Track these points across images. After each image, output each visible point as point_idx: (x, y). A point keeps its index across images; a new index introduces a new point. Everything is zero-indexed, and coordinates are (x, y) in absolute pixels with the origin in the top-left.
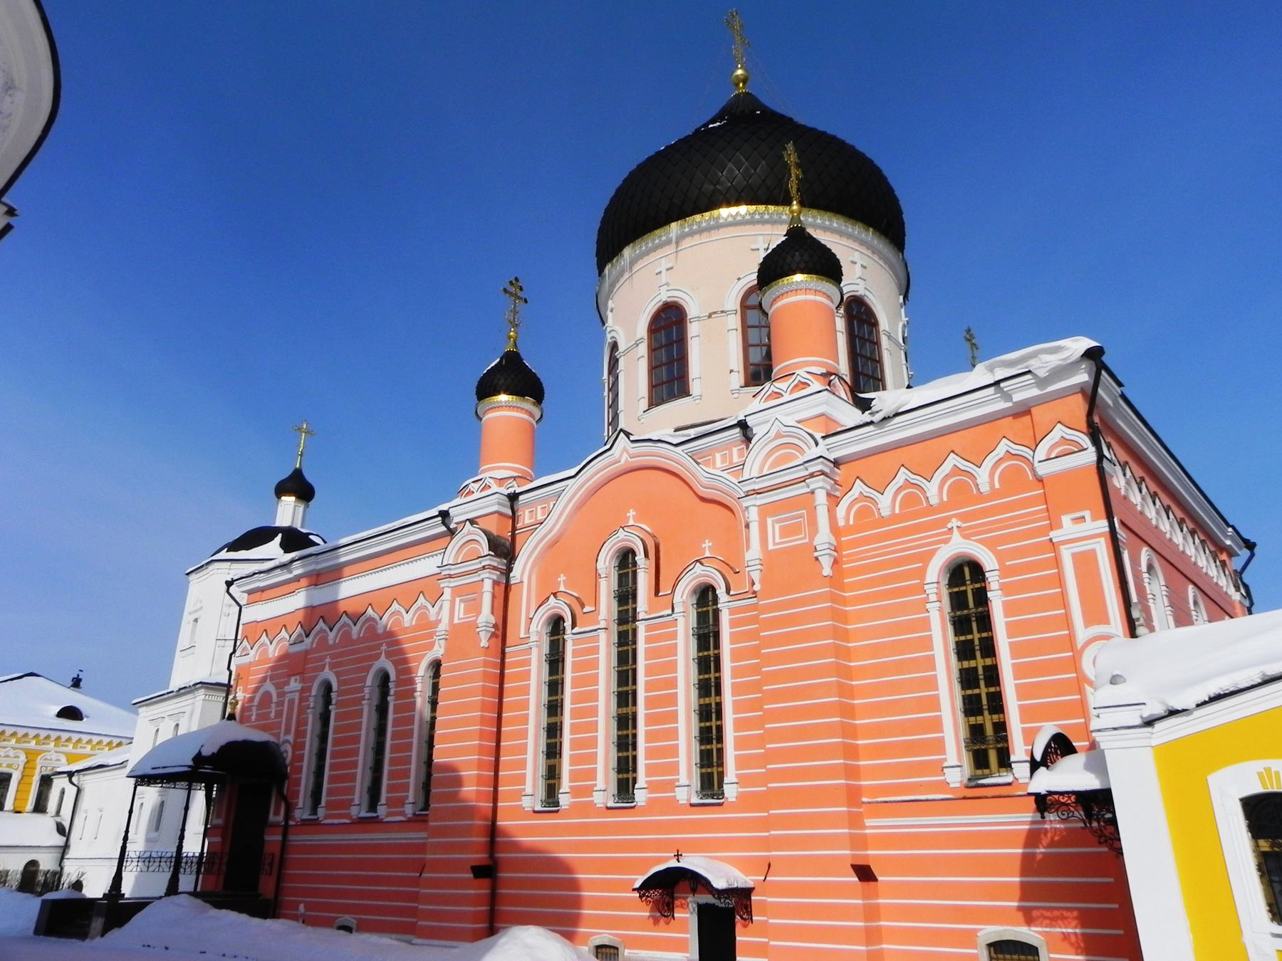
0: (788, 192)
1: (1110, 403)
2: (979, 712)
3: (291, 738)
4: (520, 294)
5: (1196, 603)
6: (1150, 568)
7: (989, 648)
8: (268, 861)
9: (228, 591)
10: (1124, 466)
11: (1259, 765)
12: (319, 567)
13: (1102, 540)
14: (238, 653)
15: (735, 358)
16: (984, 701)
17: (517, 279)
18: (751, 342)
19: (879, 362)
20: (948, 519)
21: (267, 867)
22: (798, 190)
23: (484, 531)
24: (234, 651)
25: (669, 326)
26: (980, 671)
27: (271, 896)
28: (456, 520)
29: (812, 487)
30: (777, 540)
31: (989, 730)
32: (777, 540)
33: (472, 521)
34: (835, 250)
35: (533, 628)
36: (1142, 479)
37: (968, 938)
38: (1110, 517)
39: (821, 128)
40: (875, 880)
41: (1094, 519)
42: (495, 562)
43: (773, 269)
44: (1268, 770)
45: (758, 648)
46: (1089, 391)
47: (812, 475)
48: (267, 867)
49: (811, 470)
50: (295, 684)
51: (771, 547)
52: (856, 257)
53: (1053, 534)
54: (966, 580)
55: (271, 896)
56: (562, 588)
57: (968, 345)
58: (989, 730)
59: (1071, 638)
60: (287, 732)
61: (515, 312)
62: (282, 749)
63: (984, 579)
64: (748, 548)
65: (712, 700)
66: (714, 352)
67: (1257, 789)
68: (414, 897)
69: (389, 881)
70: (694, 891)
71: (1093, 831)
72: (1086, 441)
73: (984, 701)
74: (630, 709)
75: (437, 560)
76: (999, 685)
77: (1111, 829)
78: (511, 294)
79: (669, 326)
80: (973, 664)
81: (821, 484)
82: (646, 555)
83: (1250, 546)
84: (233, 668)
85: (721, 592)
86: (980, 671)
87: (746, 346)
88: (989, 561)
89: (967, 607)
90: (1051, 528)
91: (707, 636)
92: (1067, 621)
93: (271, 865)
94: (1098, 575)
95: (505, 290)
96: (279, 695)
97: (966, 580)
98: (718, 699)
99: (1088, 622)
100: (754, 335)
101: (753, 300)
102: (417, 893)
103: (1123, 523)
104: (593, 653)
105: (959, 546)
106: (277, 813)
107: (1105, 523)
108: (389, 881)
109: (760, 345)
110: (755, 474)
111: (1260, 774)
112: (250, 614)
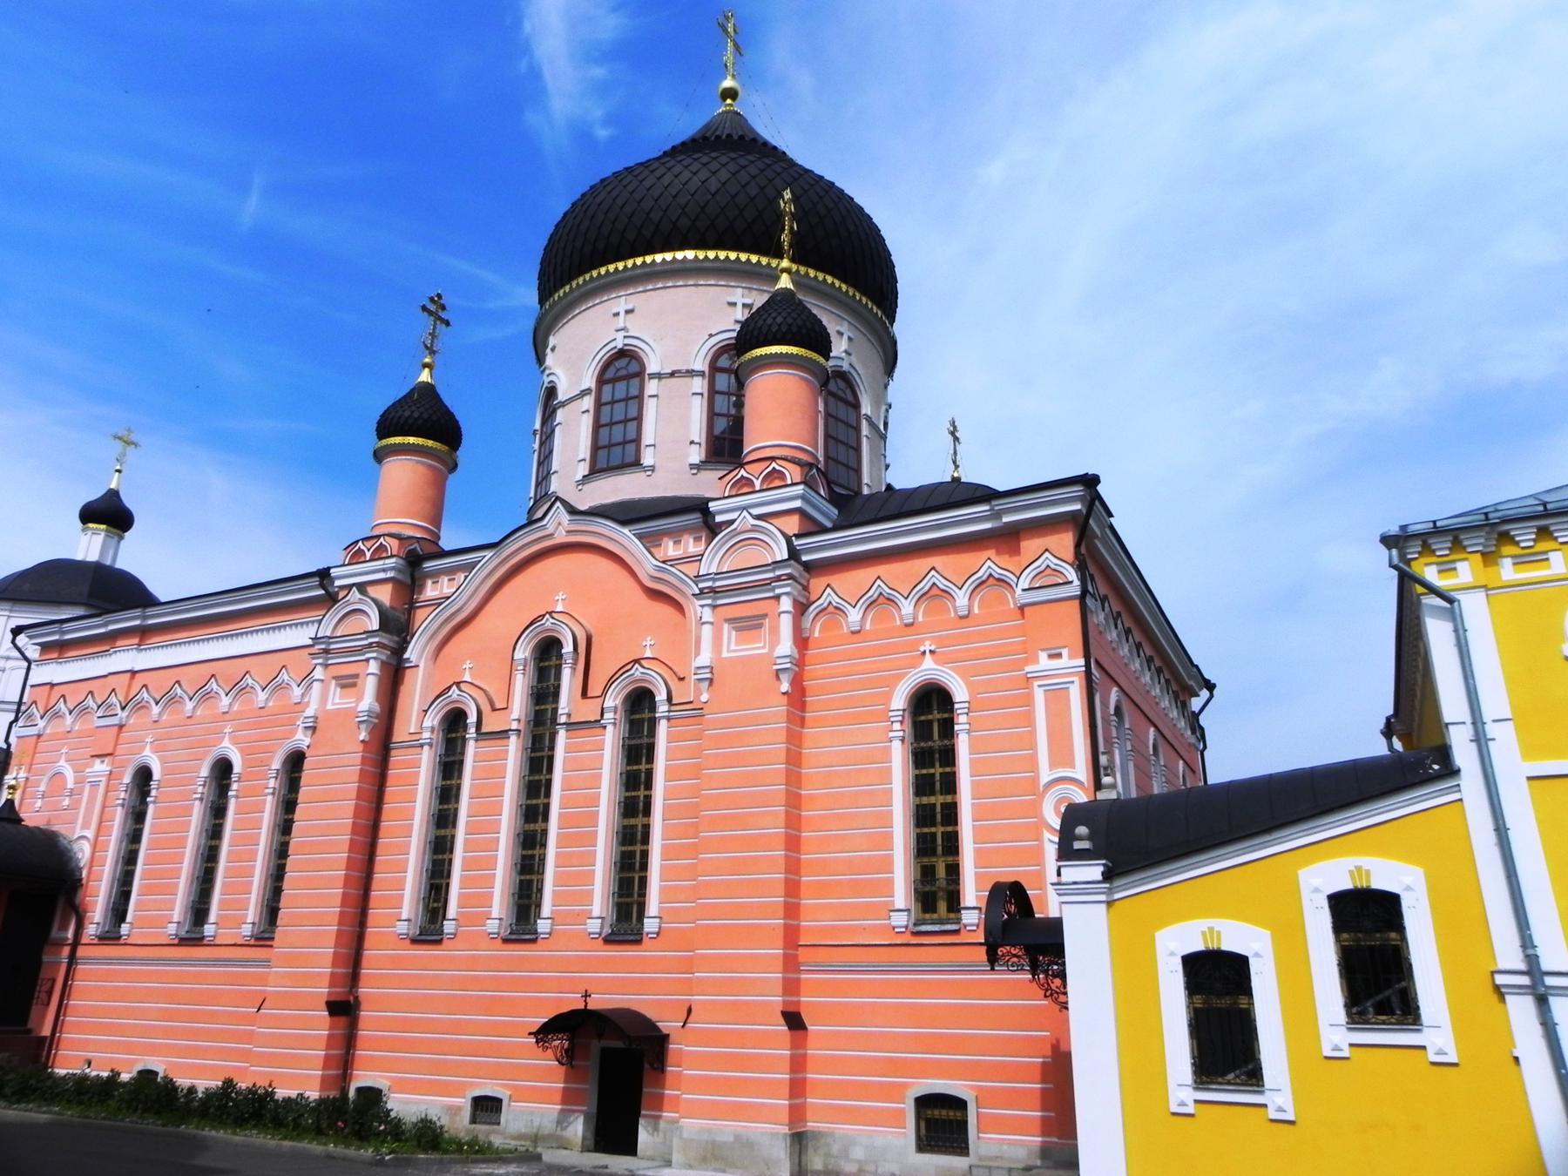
0: (780, 244)
1: (1098, 532)
2: (933, 853)
3: (90, 834)
4: (443, 315)
5: (1155, 747)
6: (1118, 710)
7: (950, 785)
8: (46, 988)
9: (13, 642)
10: (1104, 599)
11: (1203, 924)
12: (125, 658)
13: (1076, 679)
14: (20, 723)
15: (696, 427)
16: (939, 841)
17: (439, 296)
18: (717, 410)
19: (857, 450)
20: (921, 642)
21: (44, 996)
22: (791, 246)
23: (374, 600)
24: (16, 720)
25: (622, 371)
26: (938, 809)
27: (46, 1031)
28: (337, 583)
29: (778, 591)
30: (733, 647)
31: (941, 872)
32: (733, 647)
33: (362, 587)
34: (825, 320)
35: (428, 723)
36: (1119, 614)
37: (894, 1092)
38: (1087, 656)
39: (818, 171)
40: (805, 1028)
41: (1071, 657)
42: (384, 639)
43: (752, 333)
44: (1211, 929)
45: (699, 767)
46: (1081, 520)
47: (778, 578)
48: (44, 996)
49: (778, 573)
50: (101, 767)
51: (725, 654)
52: (844, 328)
53: (1028, 669)
54: (931, 706)
55: (46, 1031)
56: (467, 678)
57: (951, 438)
58: (941, 872)
59: (1036, 779)
60: (86, 826)
61: (433, 335)
62: (75, 847)
63: (952, 710)
64: (697, 654)
65: (638, 821)
66: (674, 427)
67: (1199, 946)
68: (249, 1037)
69: (213, 1017)
70: (600, 1036)
71: (1041, 985)
72: (1072, 575)
73: (939, 841)
74: (538, 826)
75: (310, 631)
76: (956, 823)
77: (1058, 982)
78: (430, 313)
79: (622, 371)
80: (932, 800)
81: (788, 589)
82: (575, 662)
83: (1211, 687)
84: (12, 739)
85: (661, 696)
86: (938, 809)
87: (712, 414)
88: (960, 693)
89: (930, 737)
90: (1027, 662)
91: (638, 753)
92: (1033, 760)
93: (50, 993)
94: (1069, 715)
95: (424, 308)
96: (79, 781)
97: (931, 706)
98: (645, 820)
99: (1053, 765)
100: (722, 404)
101: (724, 362)
102: (249, 1050)
103: (1097, 662)
104: (494, 772)
105: (929, 669)
106: (65, 927)
107: (1082, 662)
108: (213, 1017)
109: (729, 394)
110: (713, 569)
111: (1204, 933)
112: (40, 675)
